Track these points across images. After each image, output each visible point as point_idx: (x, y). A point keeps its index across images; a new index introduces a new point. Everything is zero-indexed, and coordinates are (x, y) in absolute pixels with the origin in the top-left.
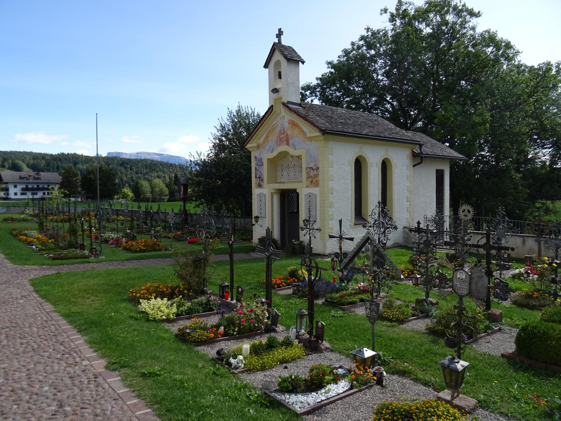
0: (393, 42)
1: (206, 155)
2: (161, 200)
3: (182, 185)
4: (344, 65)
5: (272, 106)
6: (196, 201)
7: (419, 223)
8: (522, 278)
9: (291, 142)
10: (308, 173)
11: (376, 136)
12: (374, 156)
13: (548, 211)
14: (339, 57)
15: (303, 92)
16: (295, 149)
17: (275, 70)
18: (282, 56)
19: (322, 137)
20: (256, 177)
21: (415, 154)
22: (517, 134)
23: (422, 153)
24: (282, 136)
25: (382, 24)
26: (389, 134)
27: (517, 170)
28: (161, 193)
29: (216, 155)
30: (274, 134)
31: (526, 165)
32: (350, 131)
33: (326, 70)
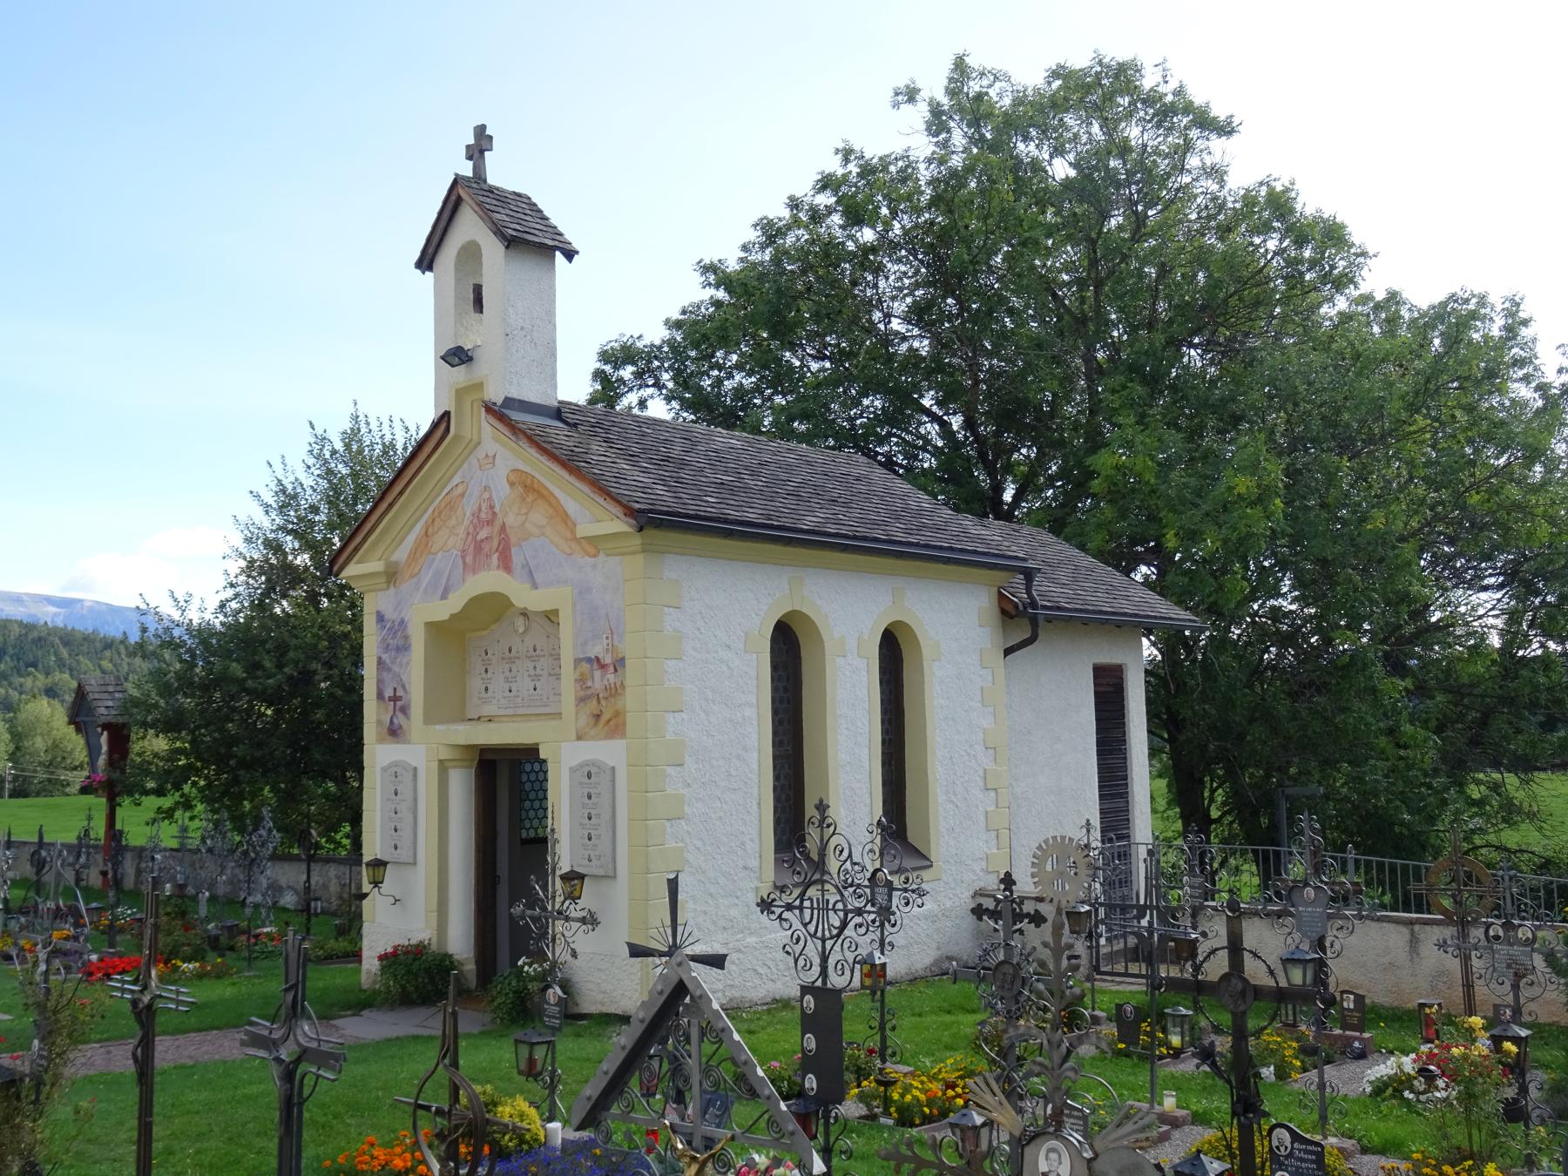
0: (935, 202)
1: (213, 604)
2: (52, 787)
3: (106, 726)
4: (762, 277)
5: (446, 415)
6: (160, 792)
7: (1008, 881)
8: (1407, 1094)
9: (517, 560)
10: (581, 680)
11: (855, 538)
12: (848, 615)
13: (1511, 813)
14: (745, 248)
15: (608, 368)
16: (535, 586)
17: (458, 280)
18: (492, 230)
19: (637, 541)
20: (380, 696)
21: (1009, 608)
22: (1382, 538)
23: (1034, 604)
24: (483, 534)
25: (902, 137)
26: (908, 532)
27: (1396, 666)
28: (57, 758)
29: (261, 606)
30: (453, 522)
31: (1428, 647)
32: (751, 516)
33: (697, 293)
